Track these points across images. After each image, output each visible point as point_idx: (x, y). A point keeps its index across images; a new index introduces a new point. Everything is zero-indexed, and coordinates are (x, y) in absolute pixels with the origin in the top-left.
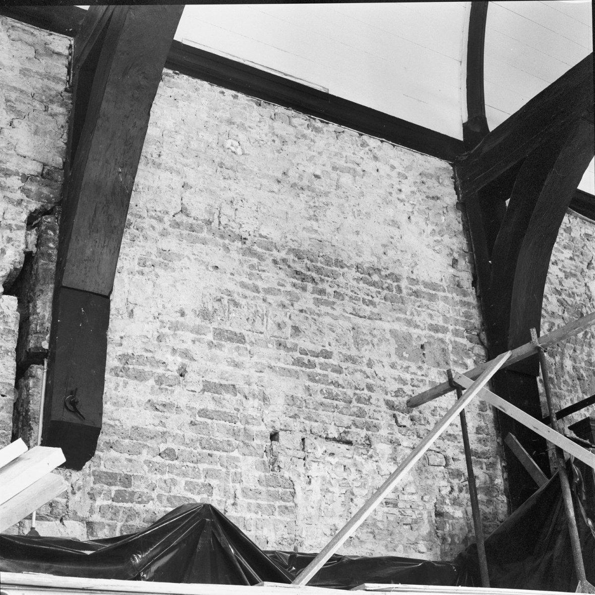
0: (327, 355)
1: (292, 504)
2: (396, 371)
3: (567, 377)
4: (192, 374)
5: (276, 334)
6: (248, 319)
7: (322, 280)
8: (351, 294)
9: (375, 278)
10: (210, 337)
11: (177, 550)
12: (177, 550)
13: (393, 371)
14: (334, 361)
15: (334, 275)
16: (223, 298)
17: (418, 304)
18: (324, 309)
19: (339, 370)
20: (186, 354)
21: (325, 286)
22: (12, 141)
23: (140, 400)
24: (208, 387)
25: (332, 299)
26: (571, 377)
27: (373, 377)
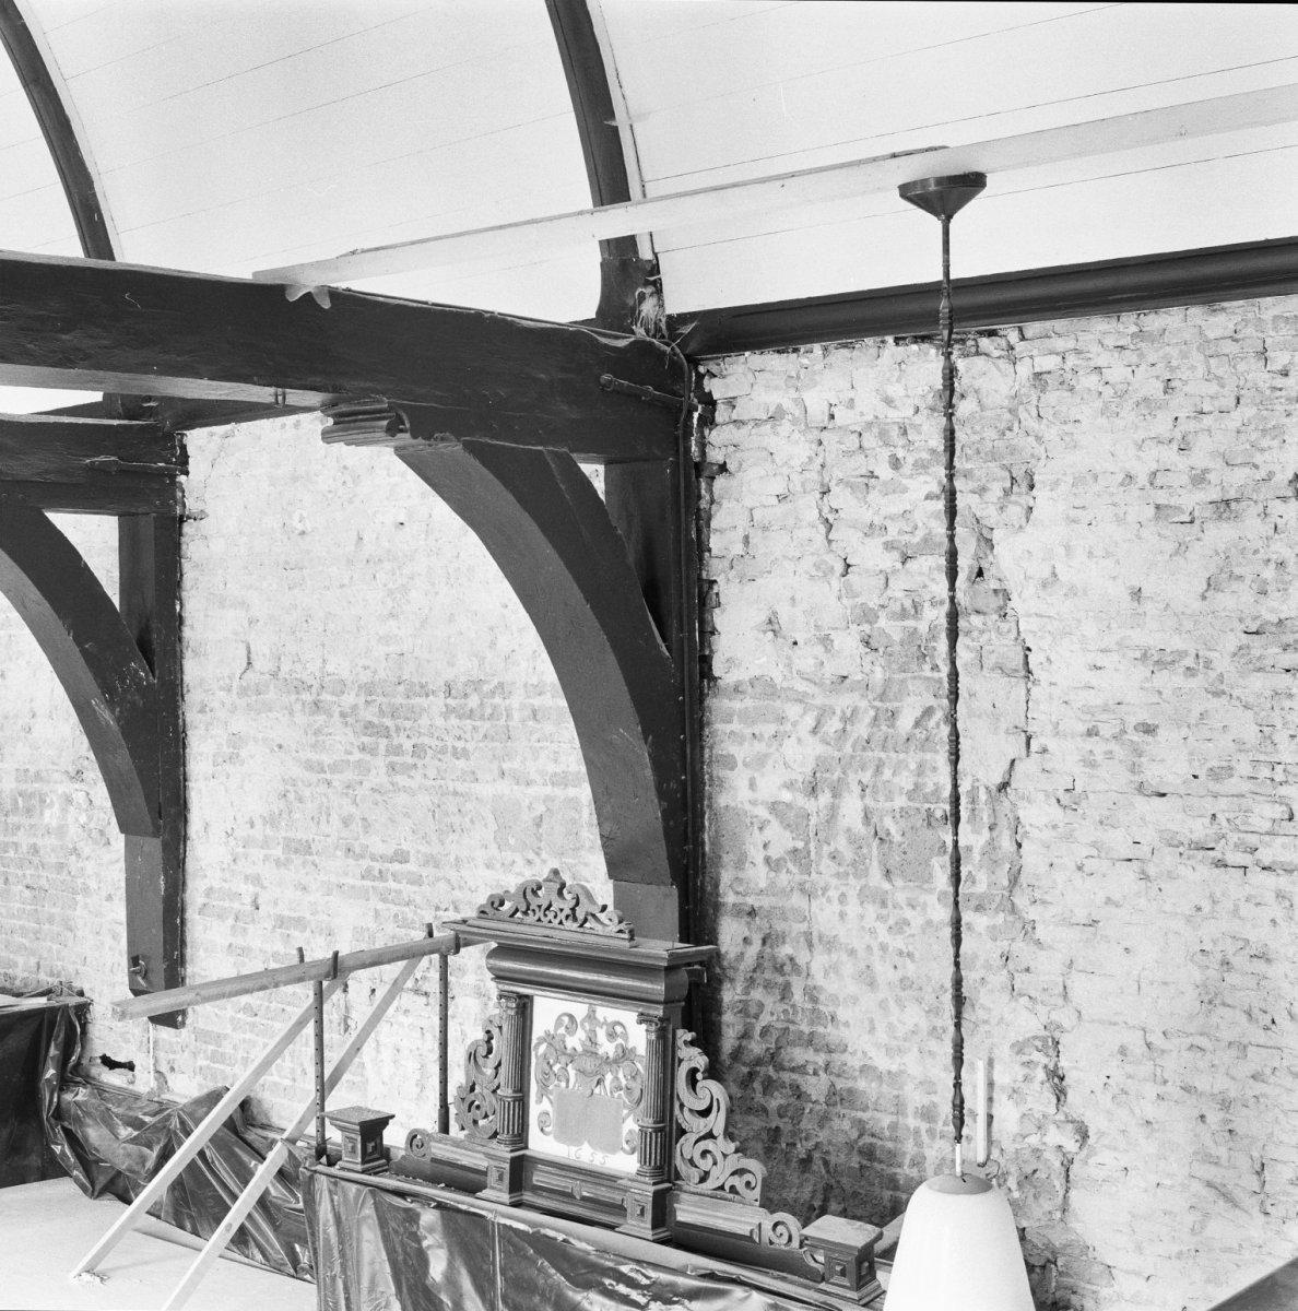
0: (401, 857)
1: (359, 1079)
2: (493, 872)
3: (841, 843)
4: (1291, 494)
5: (343, 835)
6: (312, 818)
7: (398, 729)
8: (434, 743)
9: (473, 701)
10: (278, 852)
11: (237, 1150)
12: (237, 1150)
13: (488, 873)
14: (411, 867)
15: (414, 714)
16: (288, 791)
17: (536, 736)
18: (401, 780)
19: (417, 881)
20: (256, 880)
21: (401, 739)
22: (452, 837)
23: (832, 641)
24: (281, 922)
25: (410, 761)
26: (853, 840)
27: (460, 887)
